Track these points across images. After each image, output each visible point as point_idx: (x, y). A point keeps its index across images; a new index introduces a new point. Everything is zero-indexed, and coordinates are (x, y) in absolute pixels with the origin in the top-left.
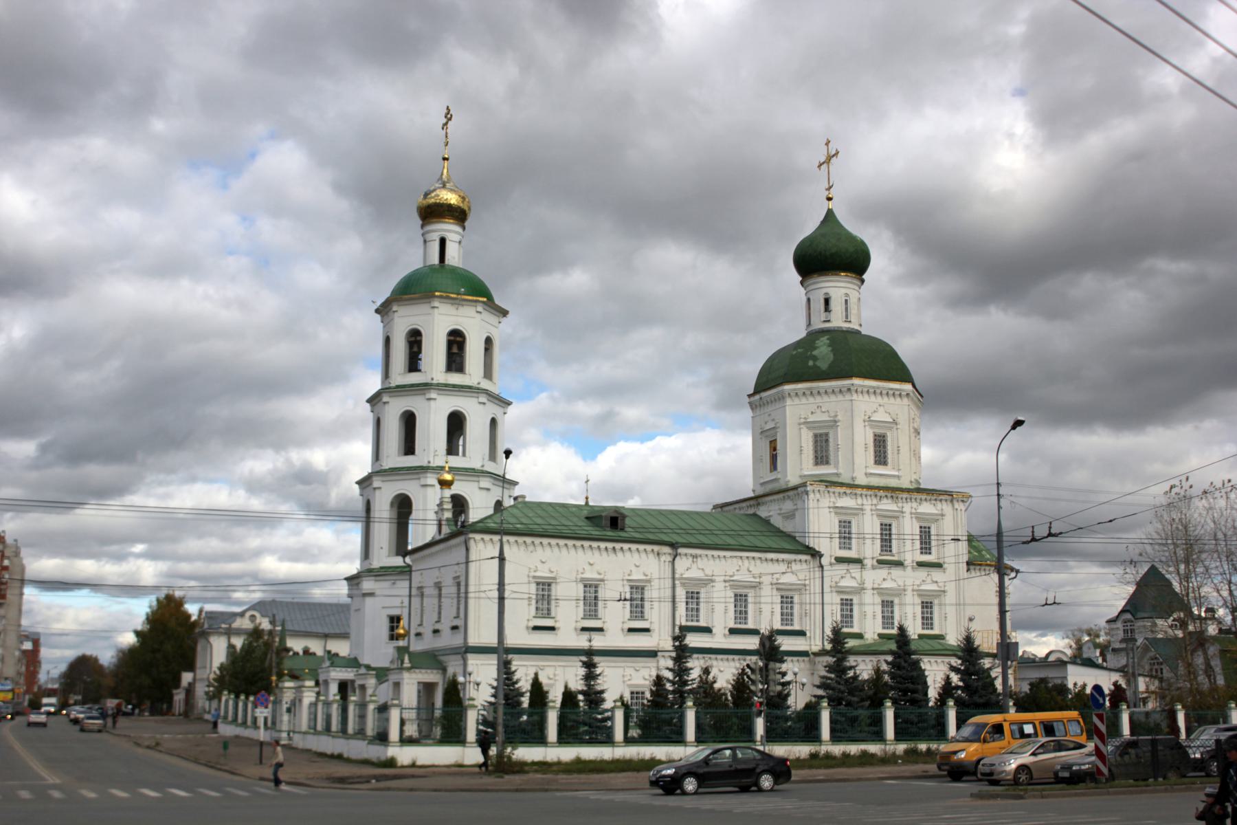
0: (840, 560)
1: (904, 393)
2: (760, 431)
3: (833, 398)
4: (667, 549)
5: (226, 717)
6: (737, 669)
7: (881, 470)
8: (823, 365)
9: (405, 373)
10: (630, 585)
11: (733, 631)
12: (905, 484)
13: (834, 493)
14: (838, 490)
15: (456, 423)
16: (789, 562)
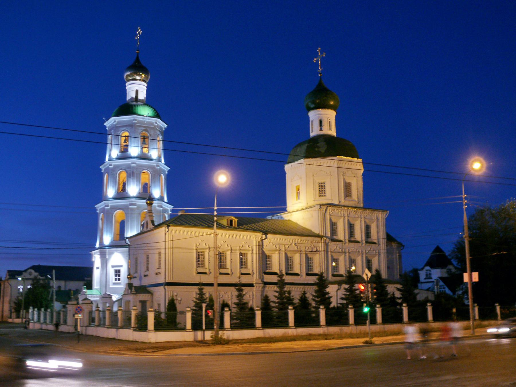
5: (33, 319)
6: (301, 291)
11: (308, 274)
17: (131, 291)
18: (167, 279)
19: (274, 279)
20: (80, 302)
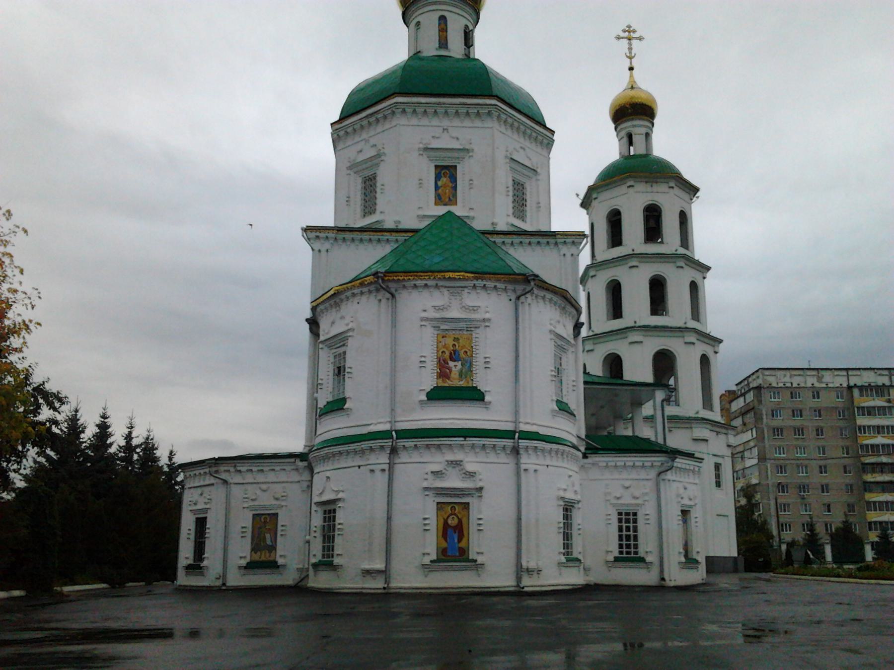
9: (608, 248)
10: (476, 566)
15: (657, 287)
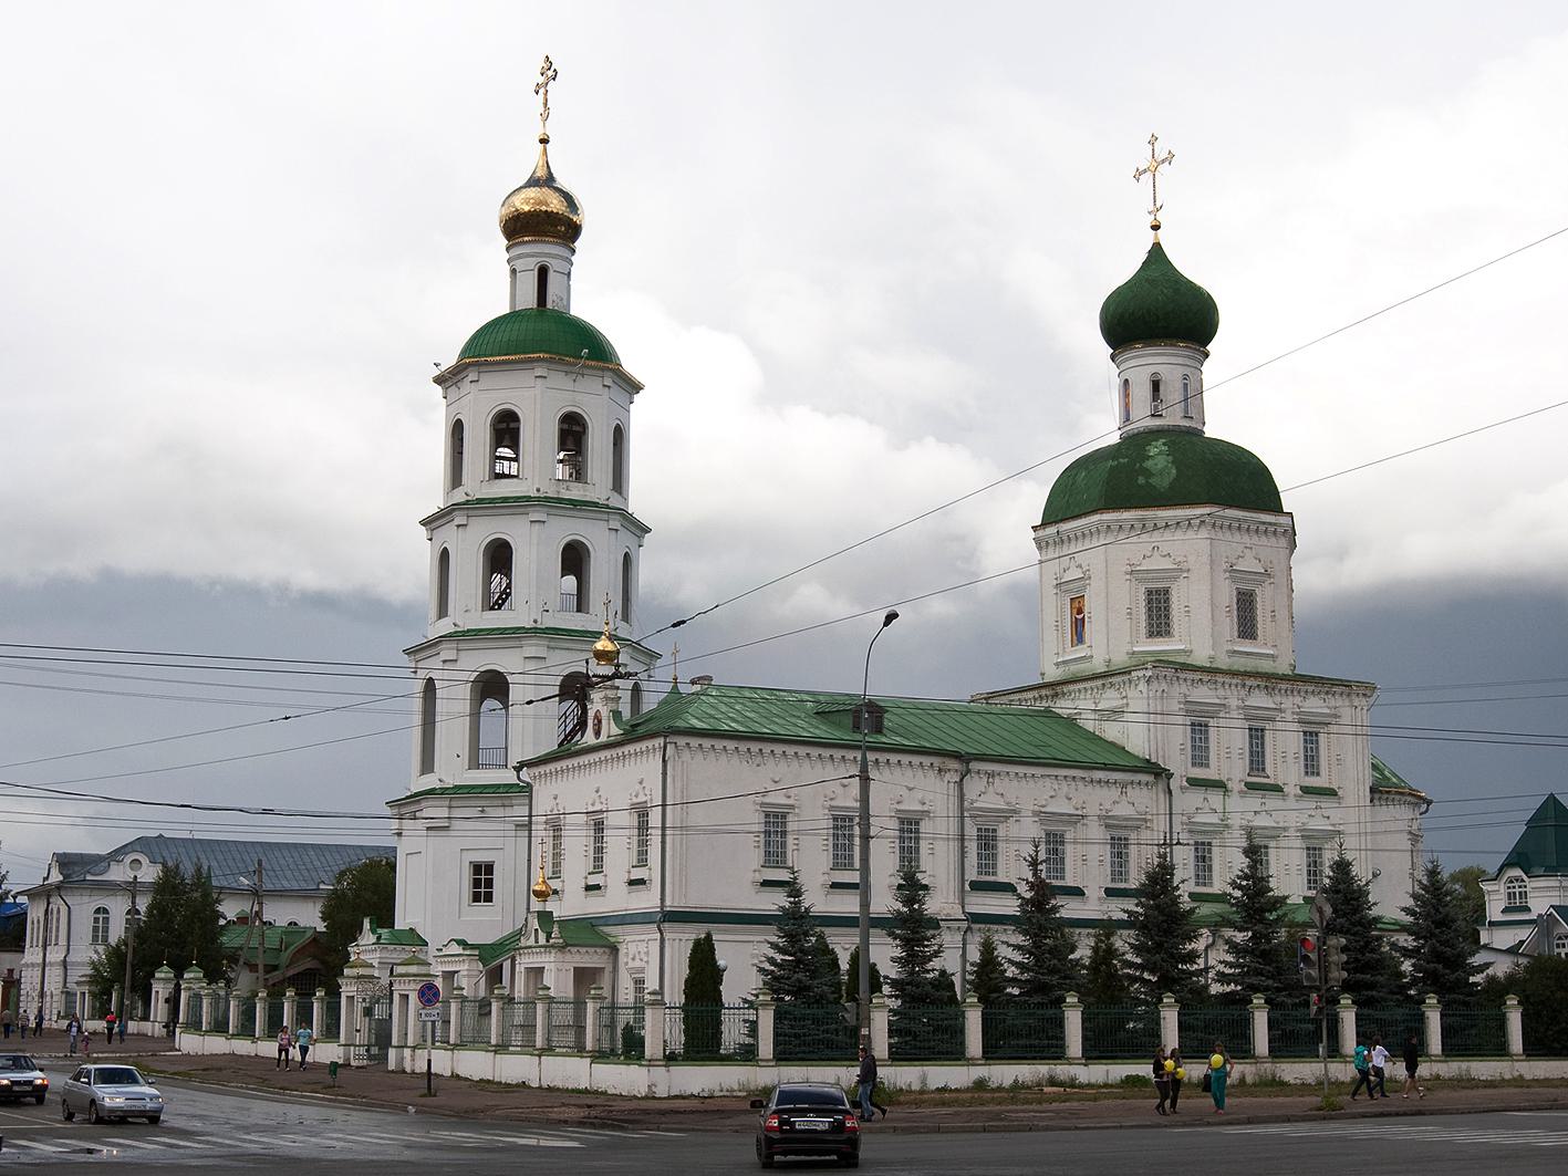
0: (1194, 783)
1: (1280, 530)
2: (1055, 582)
3: (1179, 535)
4: (953, 764)
7: (1247, 646)
8: (1162, 483)
11: (1110, 892)
12: (1284, 669)
13: (1185, 680)
14: (1190, 676)
16: (1124, 786)
17: (548, 938)
18: (668, 903)
19: (1008, 906)
20: (848, 905)
